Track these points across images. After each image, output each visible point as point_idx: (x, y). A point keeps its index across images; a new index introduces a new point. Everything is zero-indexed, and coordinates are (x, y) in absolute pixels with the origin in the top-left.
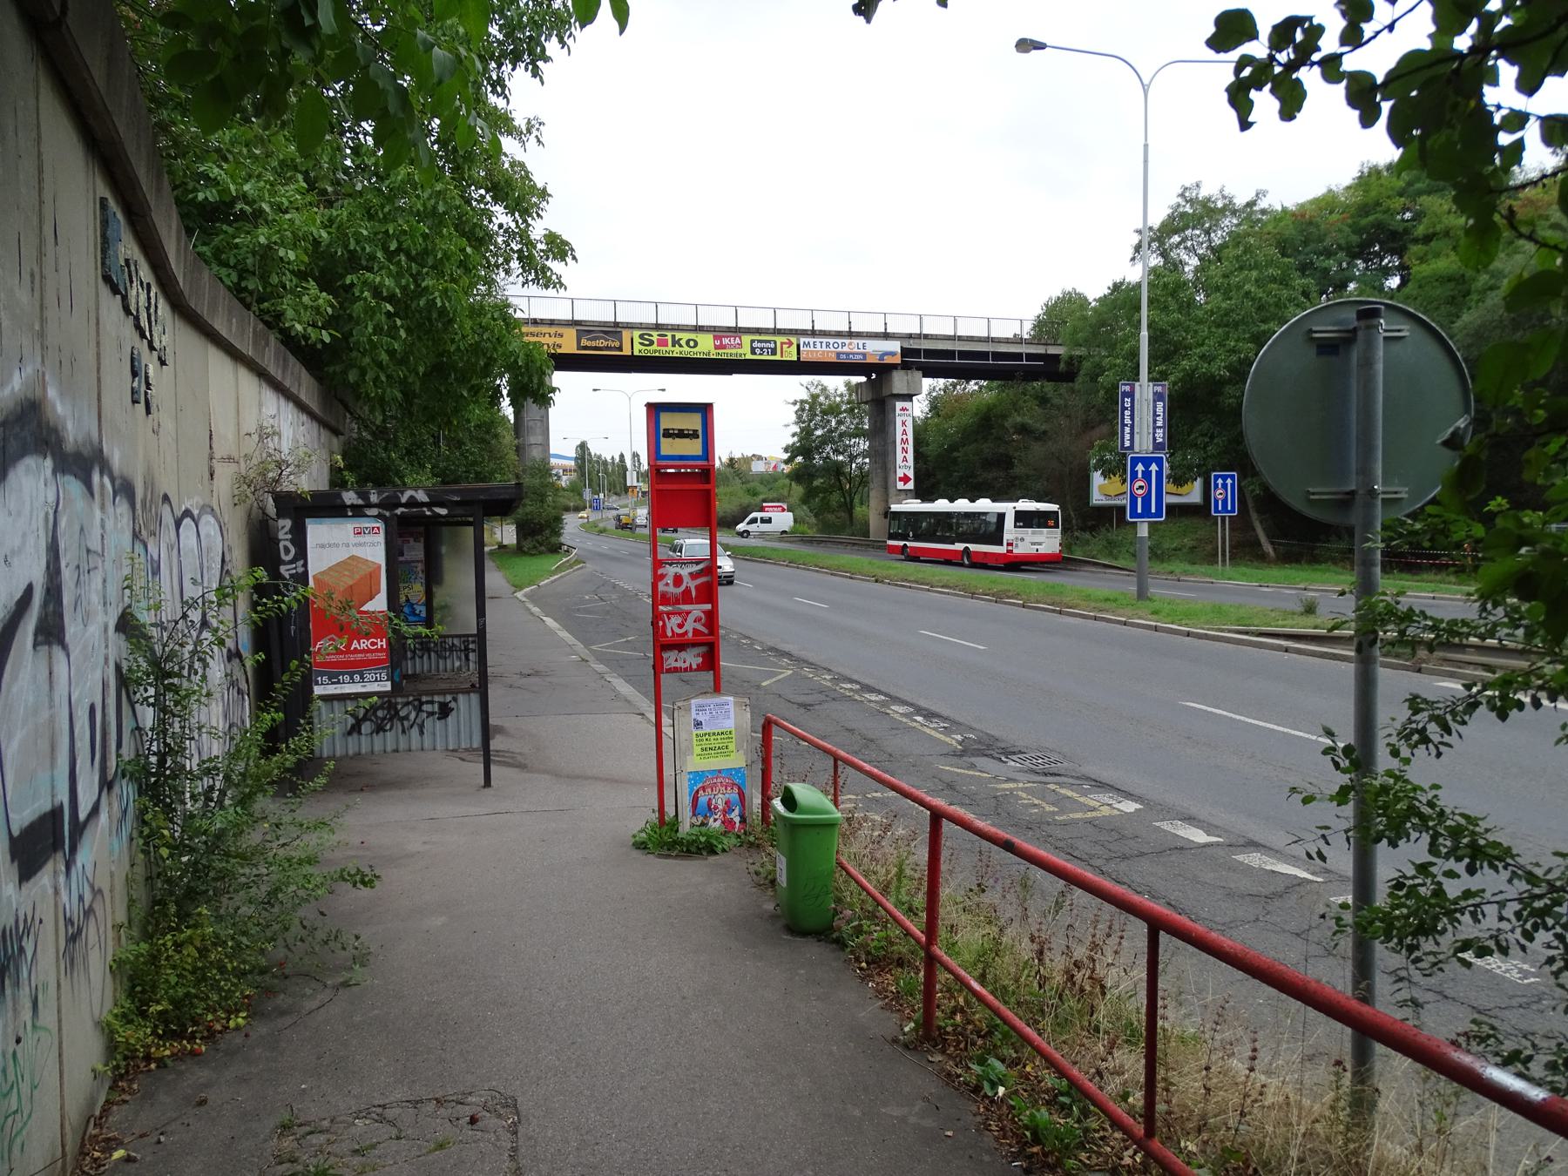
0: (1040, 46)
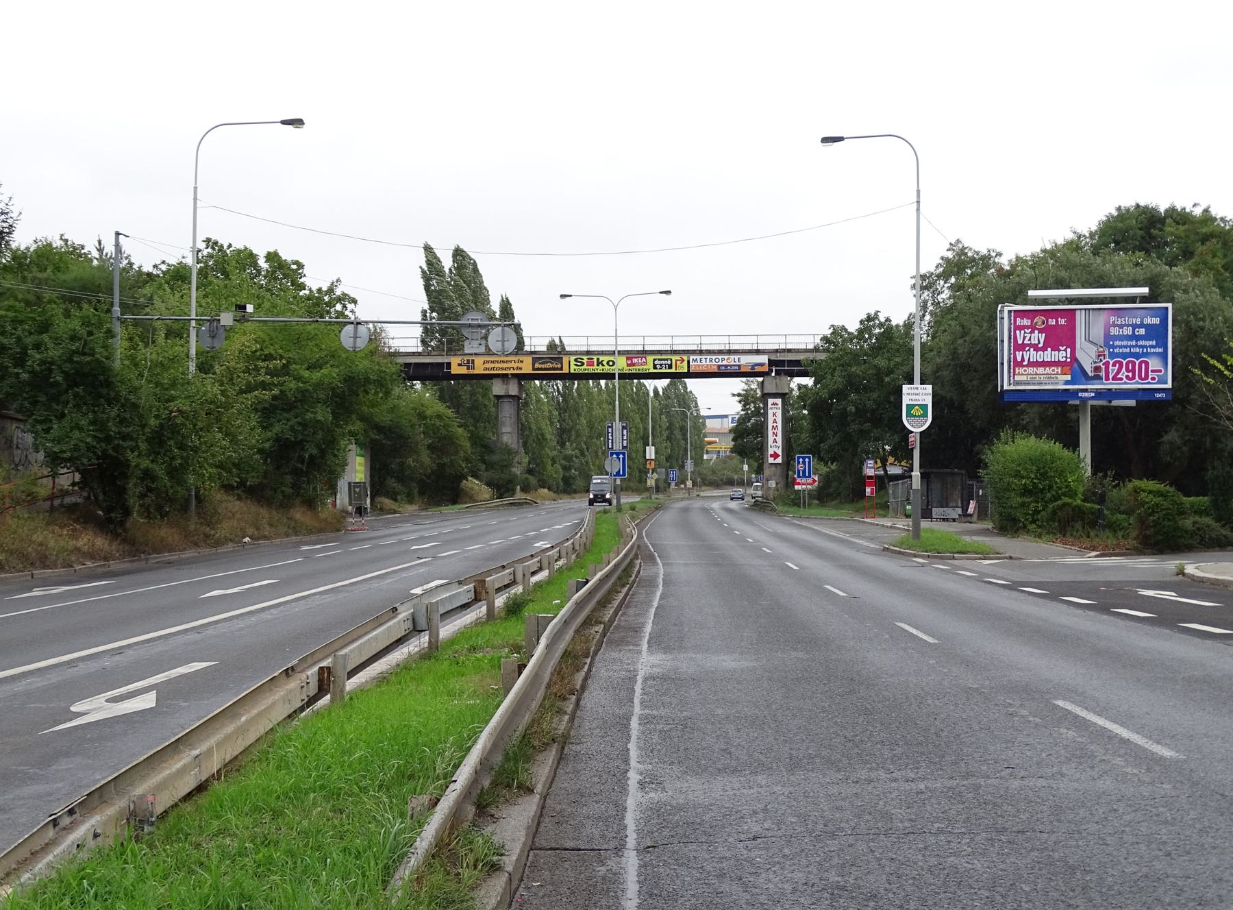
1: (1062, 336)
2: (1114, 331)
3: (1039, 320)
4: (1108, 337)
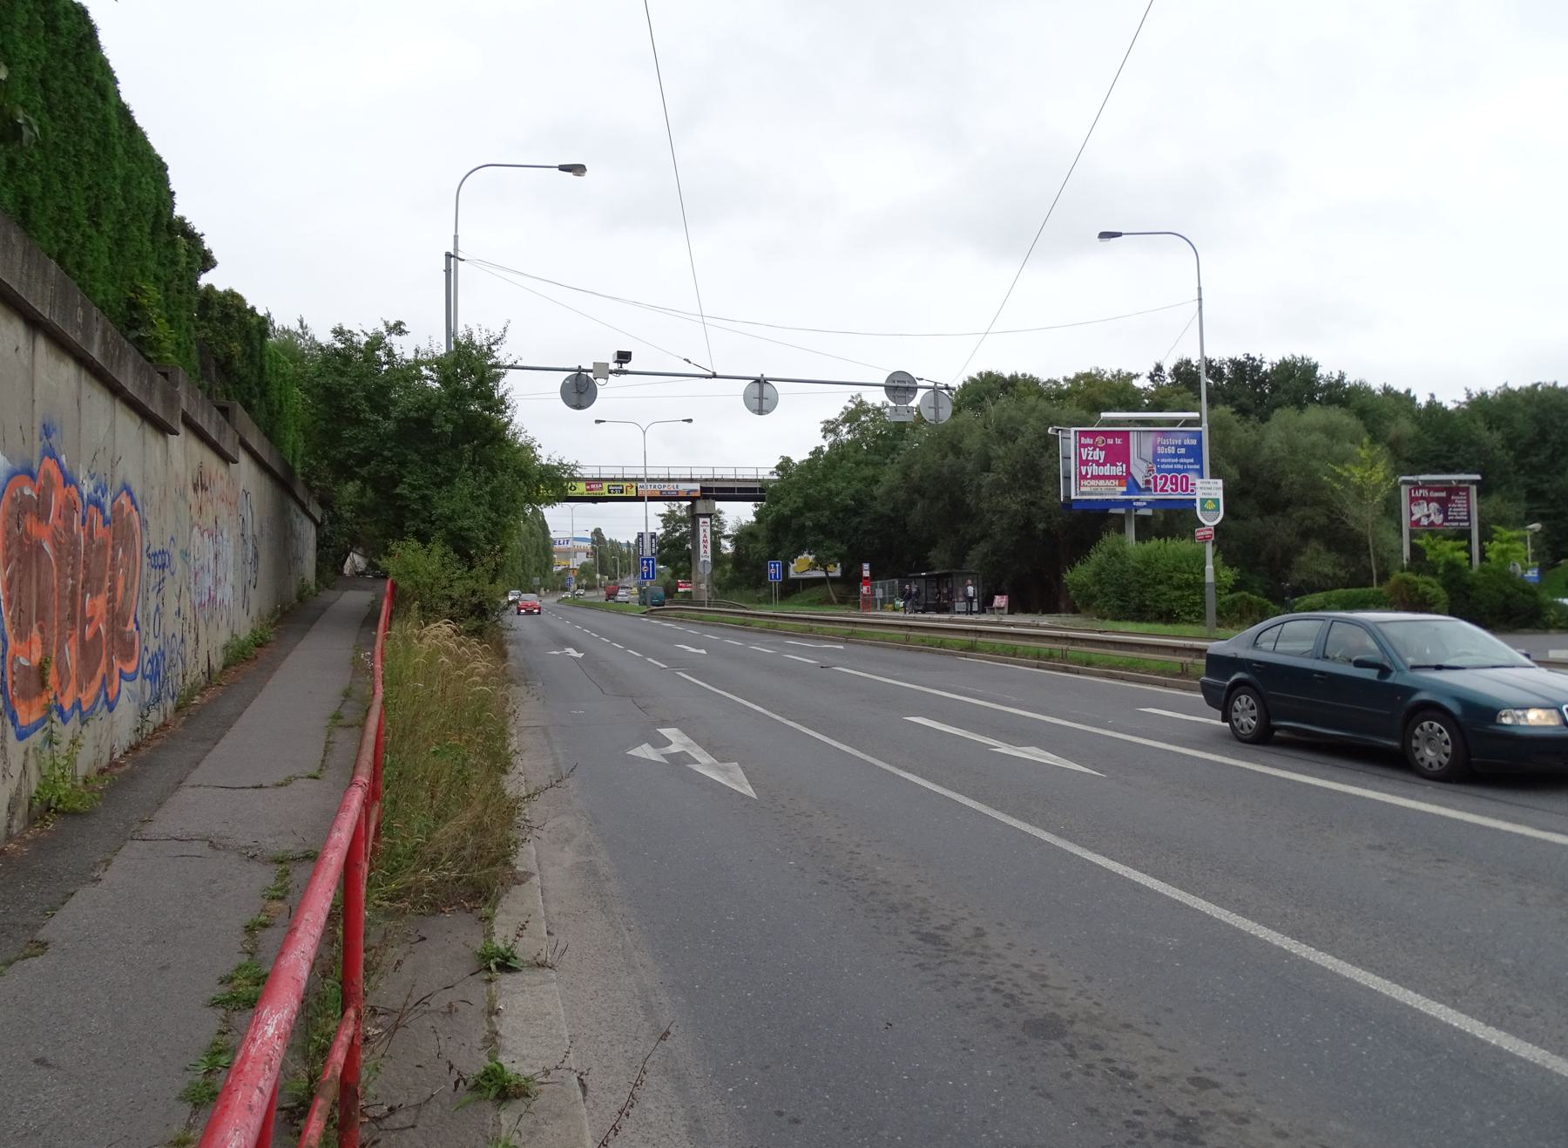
0: (563, 168)
1: (1118, 454)
2: (1160, 450)
3: (1100, 439)
4: (1156, 455)
